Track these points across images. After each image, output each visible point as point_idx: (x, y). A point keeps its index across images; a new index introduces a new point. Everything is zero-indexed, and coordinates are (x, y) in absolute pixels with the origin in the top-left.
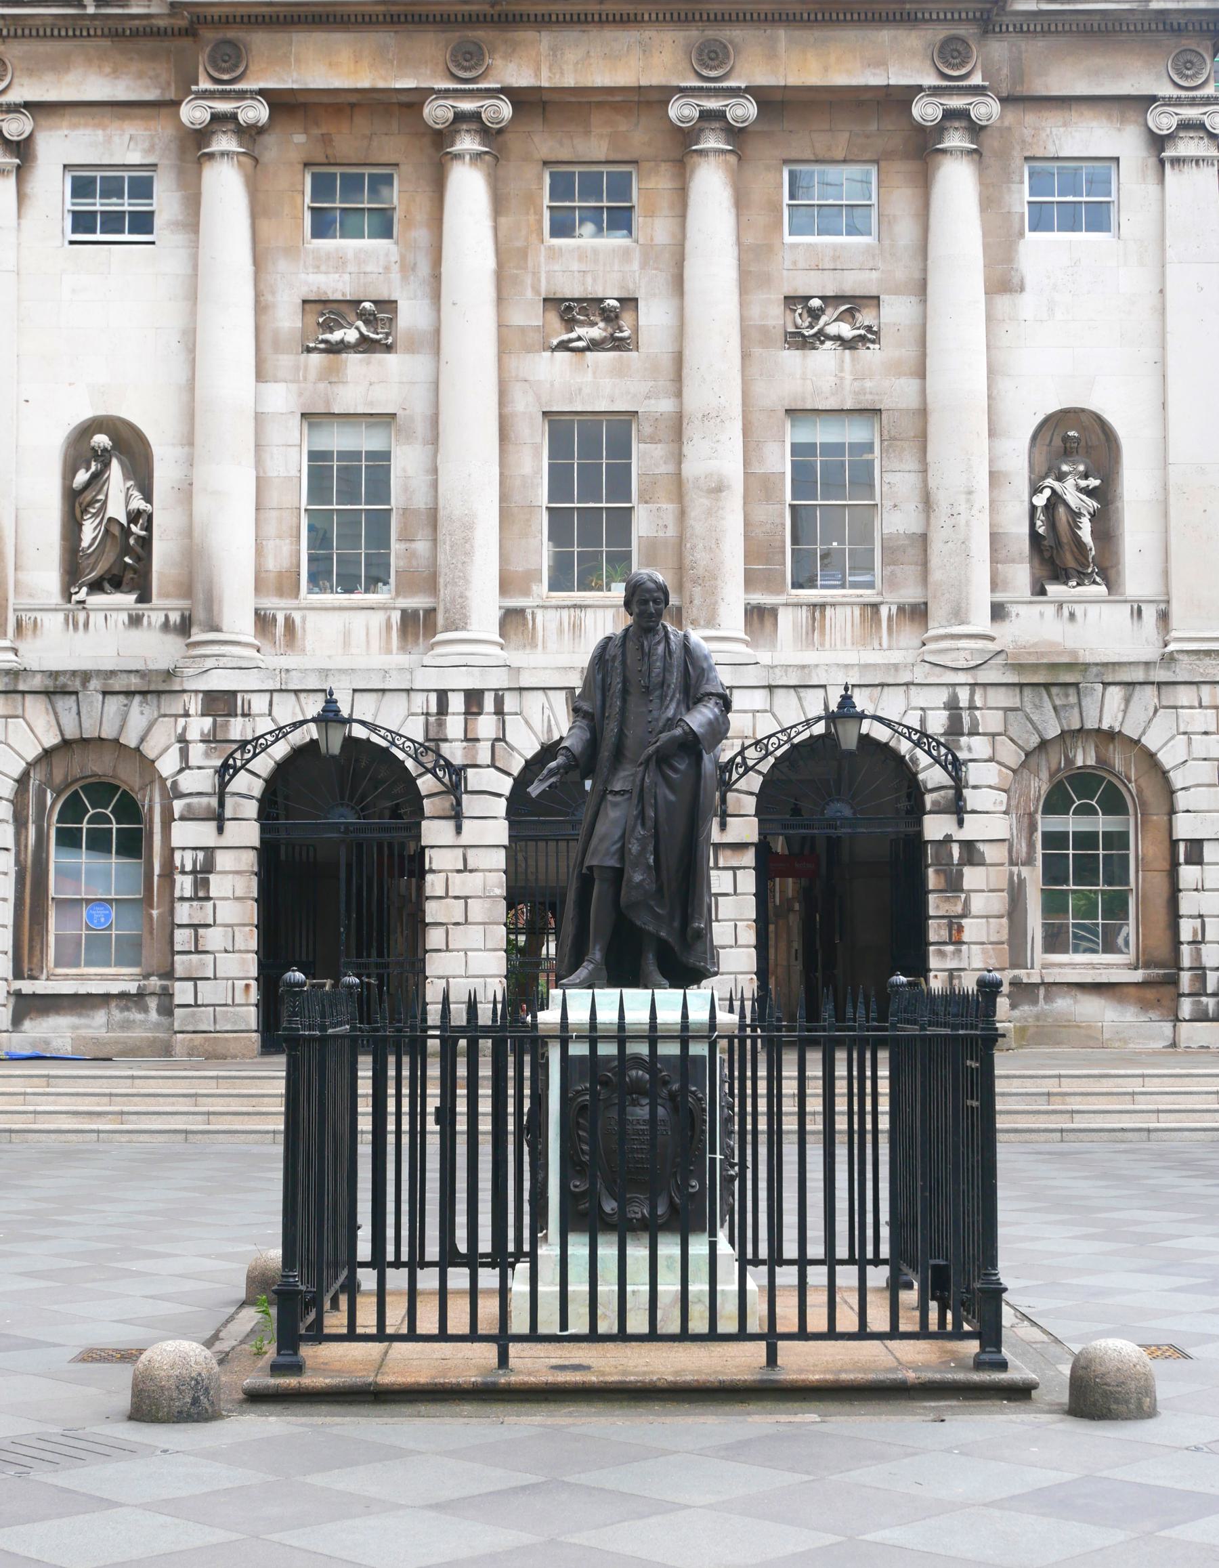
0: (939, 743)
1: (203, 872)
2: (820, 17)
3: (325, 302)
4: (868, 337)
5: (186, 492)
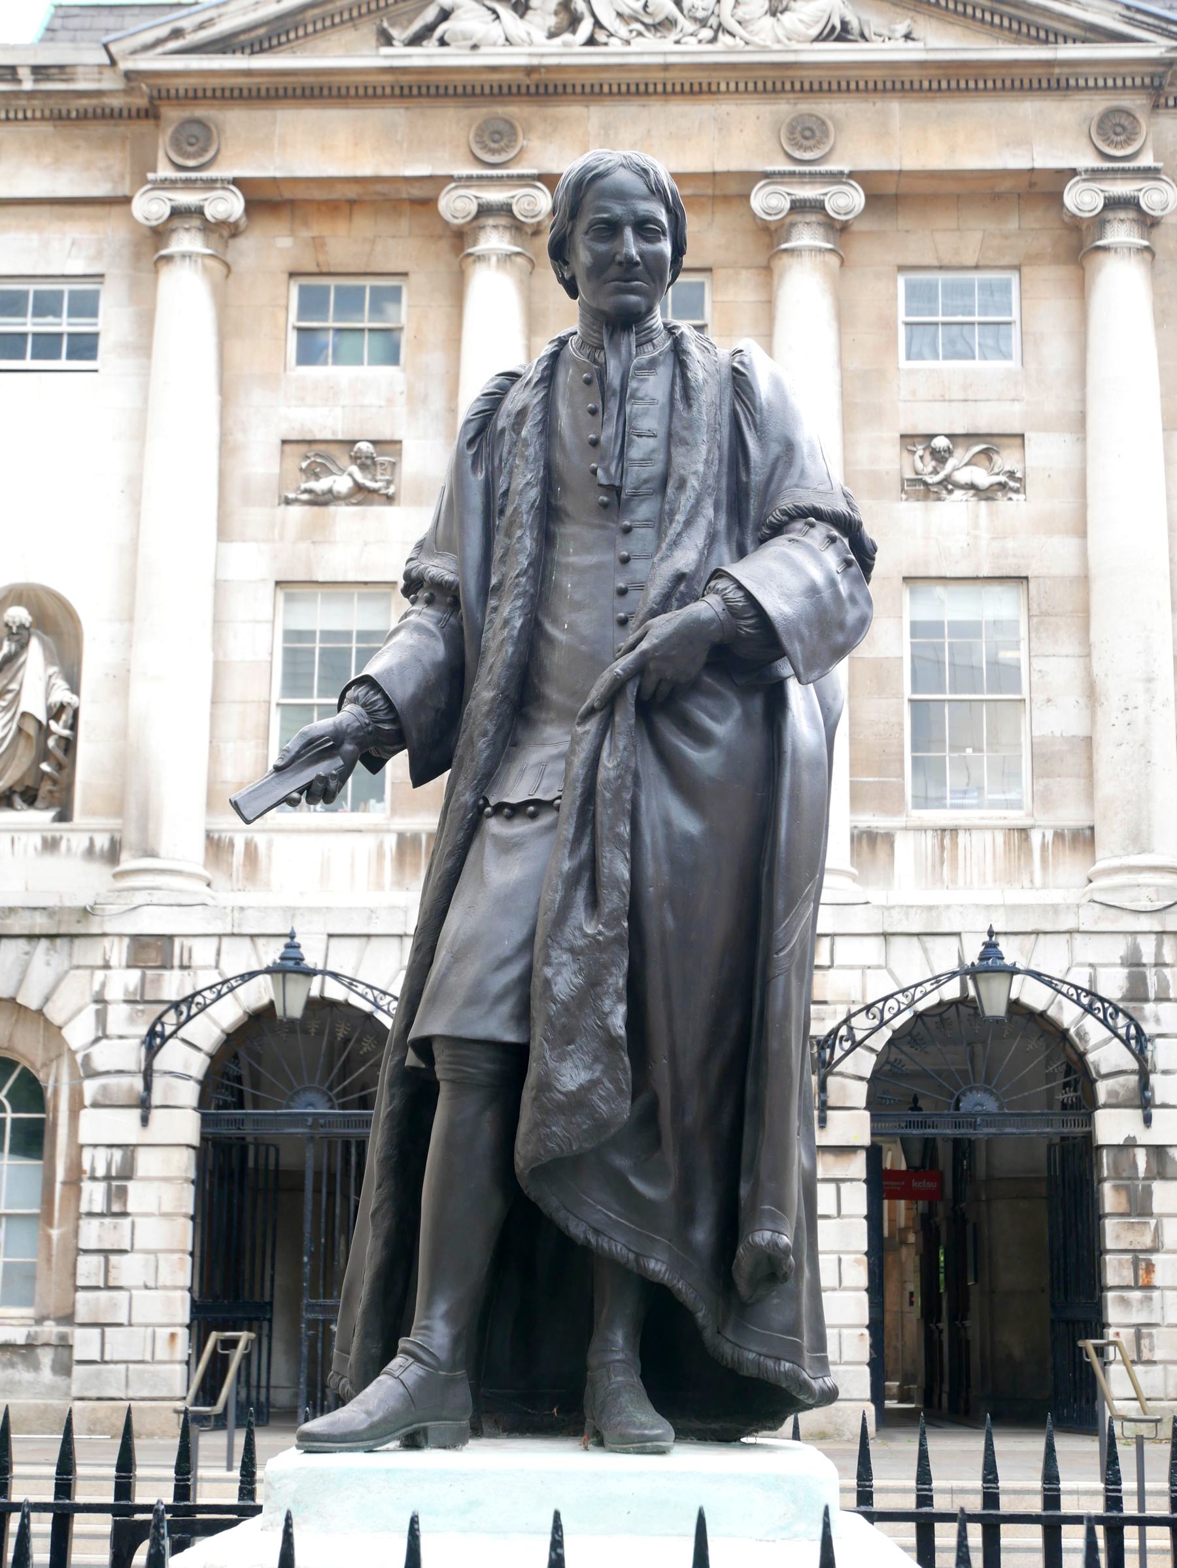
0: (1117, 1010)
1: (120, 1179)
2: (944, 85)
3: (310, 442)
5: (122, 681)
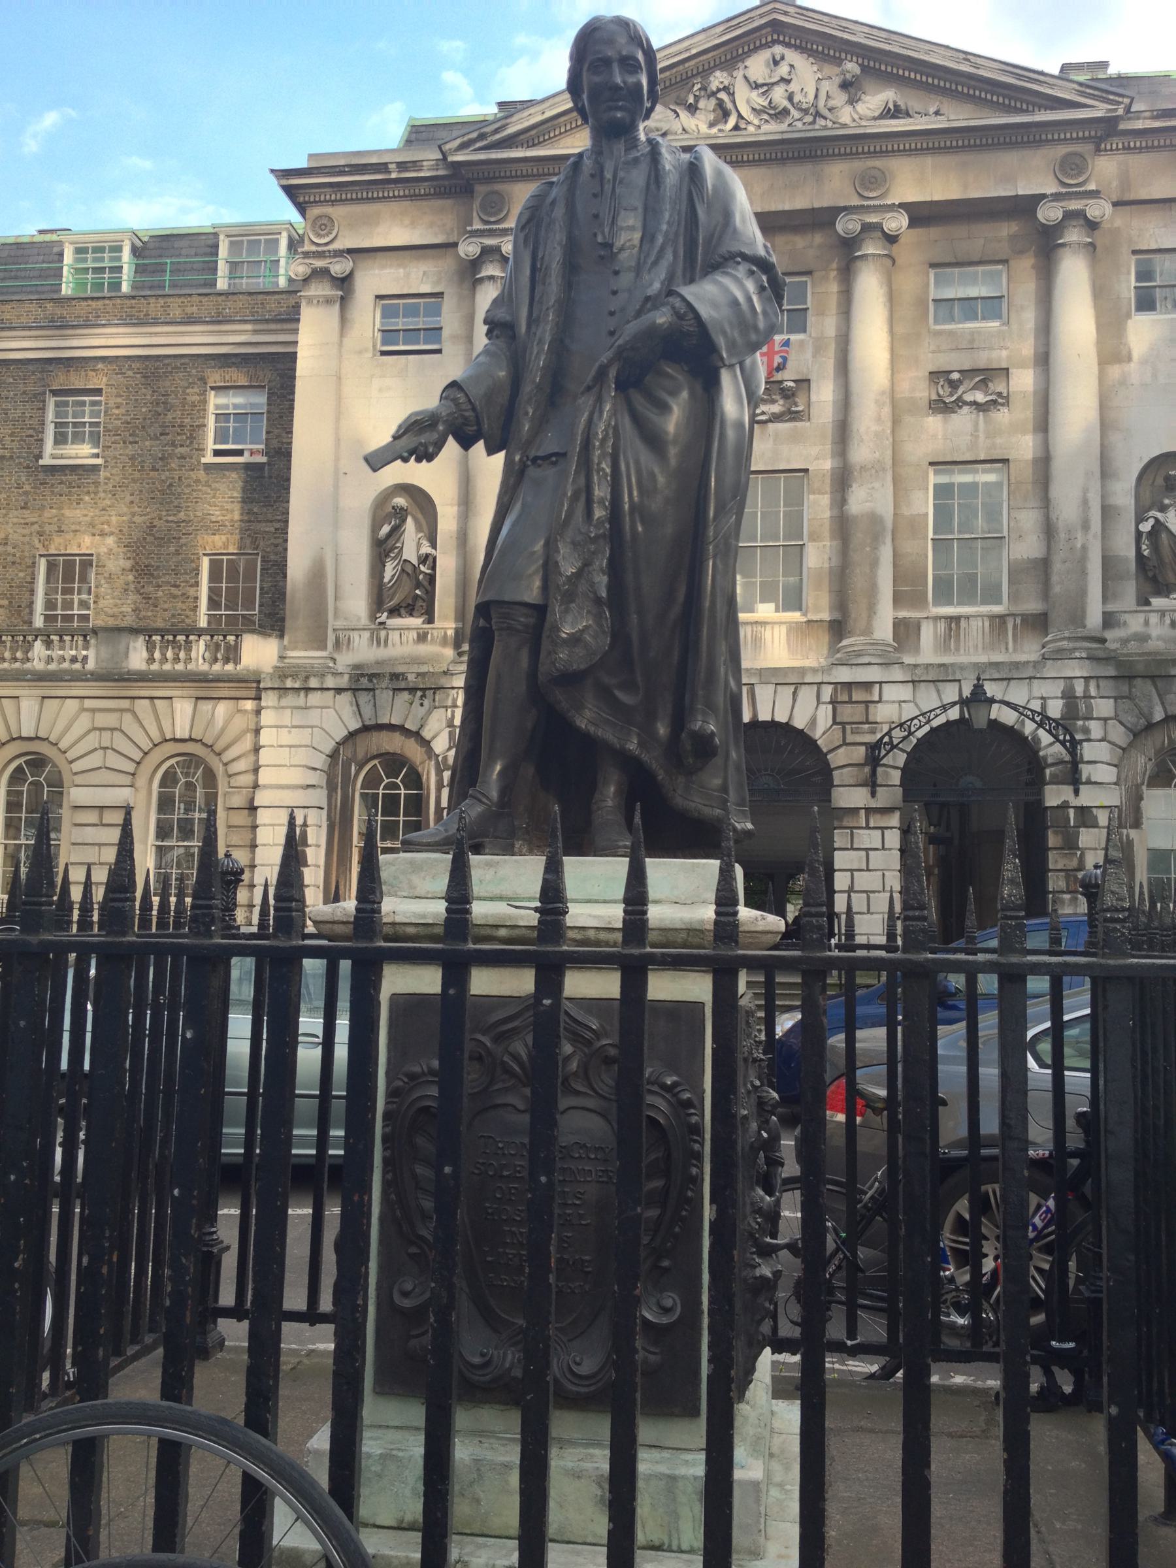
0: (1058, 724)
4: (1001, 401)
